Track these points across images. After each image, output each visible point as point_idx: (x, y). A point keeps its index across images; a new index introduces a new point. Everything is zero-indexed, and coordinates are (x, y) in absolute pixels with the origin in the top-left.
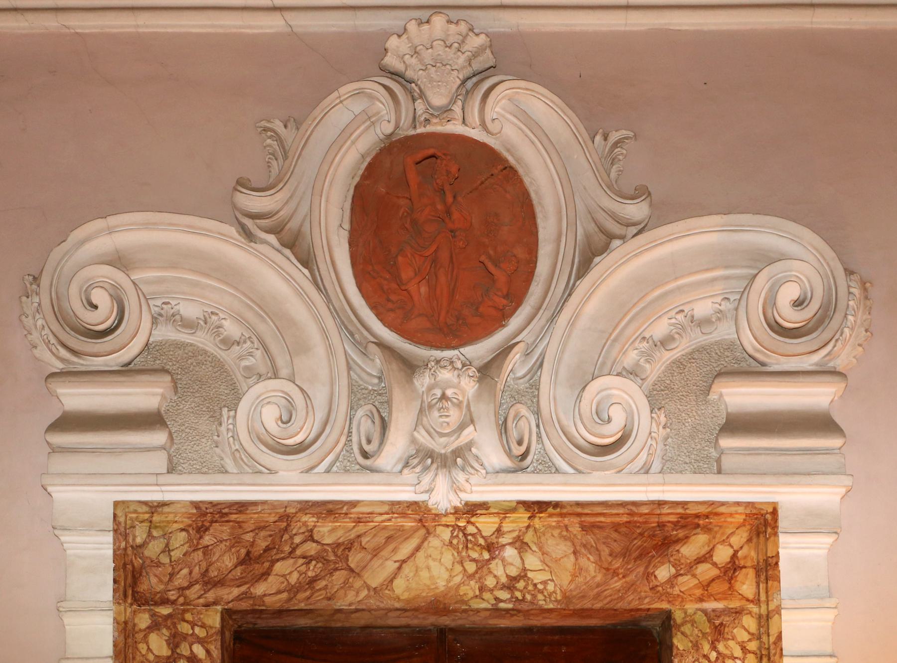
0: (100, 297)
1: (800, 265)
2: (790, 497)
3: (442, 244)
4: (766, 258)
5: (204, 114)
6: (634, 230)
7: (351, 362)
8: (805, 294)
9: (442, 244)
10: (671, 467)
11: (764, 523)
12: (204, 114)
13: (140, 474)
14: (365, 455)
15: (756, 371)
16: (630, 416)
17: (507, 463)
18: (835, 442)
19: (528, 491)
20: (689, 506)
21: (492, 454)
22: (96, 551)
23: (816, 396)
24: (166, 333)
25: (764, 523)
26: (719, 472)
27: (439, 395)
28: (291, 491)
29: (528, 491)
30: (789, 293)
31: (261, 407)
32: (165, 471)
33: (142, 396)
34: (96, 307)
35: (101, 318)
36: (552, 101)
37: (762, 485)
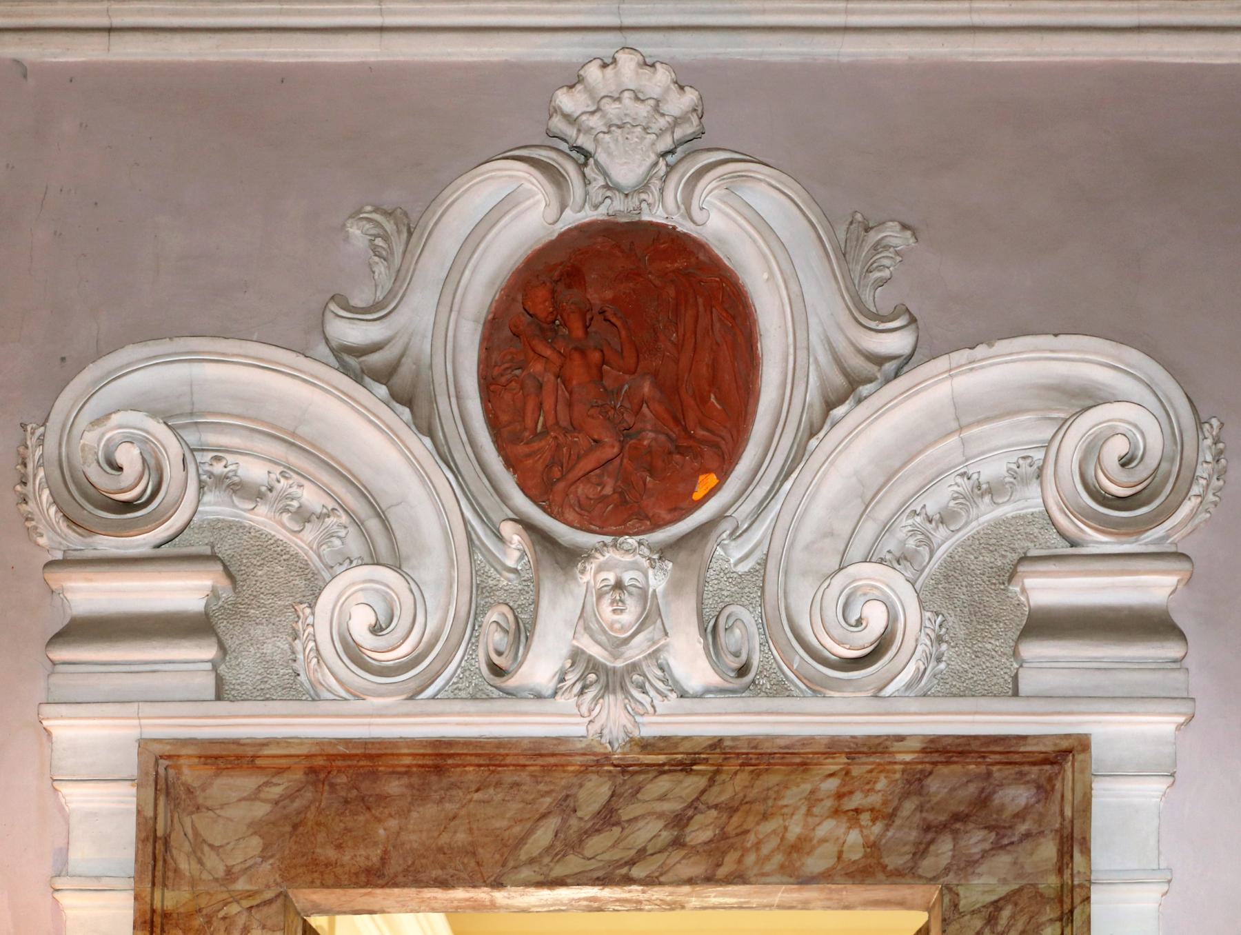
0: (129, 456)
1: (1133, 411)
2: (1113, 731)
3: (620, 376)
4: (1086, 398)
5: (254, 180)
6: (890, 367)
7: (474, 536)
8: (1136, 448)
9: (620, 376)
10: (958, 688)
11: (1060, 761)
12: (254, 180)
13: (177, 700)
14: (497, 671)
15: (1070, 554)
16: (892, 619)
17: (714, 679)
18: (1172, 650)
19: (458, 724)
20: (1029, 741)
21: (690, 662)
22: (102, 815)
23: (1153, 588)
24: (216, 507)
25: (1060, 761)
26: (1016, 693)
27: (612, 581)
28: (526, 723)
29: (458, 724)
30: (1118, 447)
31: (351, 601)
32: (213, 697)
33: (184, 591)
34: (120, 469)
35: (129, 484)
36: (780, 182)
37: (1131, 713)
